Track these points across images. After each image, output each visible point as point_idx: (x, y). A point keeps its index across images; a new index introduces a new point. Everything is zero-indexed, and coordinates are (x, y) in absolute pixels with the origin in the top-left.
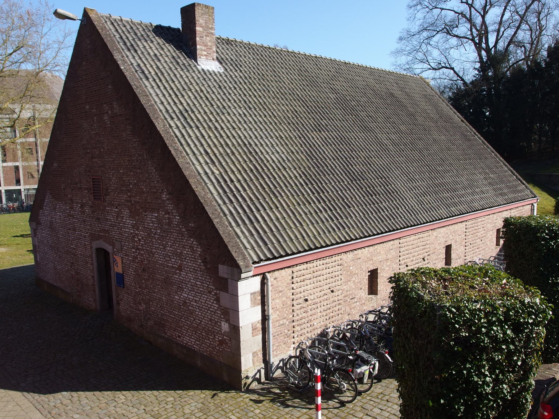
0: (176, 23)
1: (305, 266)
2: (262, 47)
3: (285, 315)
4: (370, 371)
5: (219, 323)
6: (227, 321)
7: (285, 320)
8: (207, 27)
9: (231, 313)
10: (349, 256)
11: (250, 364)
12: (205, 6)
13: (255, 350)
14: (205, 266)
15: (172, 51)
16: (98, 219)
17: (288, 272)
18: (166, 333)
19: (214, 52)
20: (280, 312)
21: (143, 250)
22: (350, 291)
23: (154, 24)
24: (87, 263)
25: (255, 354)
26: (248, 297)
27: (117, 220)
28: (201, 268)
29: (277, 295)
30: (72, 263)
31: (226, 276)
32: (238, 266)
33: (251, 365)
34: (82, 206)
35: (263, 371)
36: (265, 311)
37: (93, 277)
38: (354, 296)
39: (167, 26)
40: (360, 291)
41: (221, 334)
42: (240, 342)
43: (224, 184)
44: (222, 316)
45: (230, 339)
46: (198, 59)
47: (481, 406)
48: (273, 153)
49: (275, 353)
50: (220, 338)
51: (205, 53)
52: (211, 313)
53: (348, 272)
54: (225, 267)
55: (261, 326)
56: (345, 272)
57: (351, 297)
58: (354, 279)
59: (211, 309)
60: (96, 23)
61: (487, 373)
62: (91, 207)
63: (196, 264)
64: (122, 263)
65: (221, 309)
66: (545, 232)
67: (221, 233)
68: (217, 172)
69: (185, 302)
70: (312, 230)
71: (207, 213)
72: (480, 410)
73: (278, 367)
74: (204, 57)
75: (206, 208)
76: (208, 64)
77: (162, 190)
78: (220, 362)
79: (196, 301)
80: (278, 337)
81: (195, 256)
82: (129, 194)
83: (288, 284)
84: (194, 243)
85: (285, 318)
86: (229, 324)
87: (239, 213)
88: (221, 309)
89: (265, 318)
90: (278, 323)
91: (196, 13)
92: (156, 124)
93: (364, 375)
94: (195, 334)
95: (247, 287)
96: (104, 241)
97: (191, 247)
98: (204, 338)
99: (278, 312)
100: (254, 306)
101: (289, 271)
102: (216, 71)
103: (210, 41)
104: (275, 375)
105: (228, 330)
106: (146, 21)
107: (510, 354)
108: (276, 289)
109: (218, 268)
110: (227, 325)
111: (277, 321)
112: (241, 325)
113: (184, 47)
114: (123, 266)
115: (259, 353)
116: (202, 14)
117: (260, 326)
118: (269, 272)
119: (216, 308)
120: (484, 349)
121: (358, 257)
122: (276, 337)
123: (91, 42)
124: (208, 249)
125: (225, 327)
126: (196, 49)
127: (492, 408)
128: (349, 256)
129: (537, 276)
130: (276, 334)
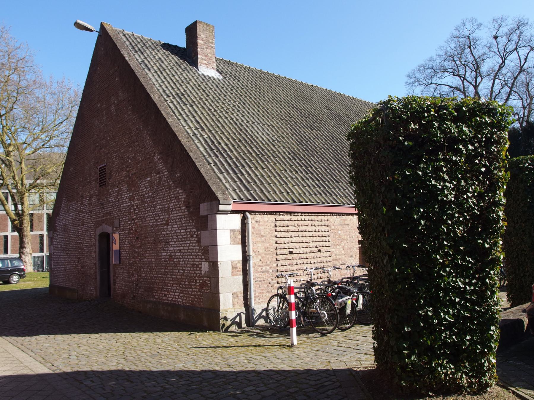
0: (182, 44)
1: (288, 217)
2: (261, 71)
3: (268, 263)
4: (352, 302)
5: (200, 266)
6: (207, 260)
7: (268, 268)
8: (208, 41)
9: (209, 252)
10: (337, 220)
11: (229, 305)
12: (206, 24)
13: (235, 291)
14: (188, 211)
15: (176, 59)
16: (102, 204)
17: (271, 219)
18: (153, 297)
19: (213, 62)
20: (262, 257)
21: (137, 219)
22: (339, 255)
23: (162, 42)
24: (91, 252)
25: (235, 296)
26: (228, 233)
27: (117, 198)
28: (184, 215)
29: (259, 239)
30: (79, 258)
31: (206, 214)
32: (216, 199)
33: (231, 306)
34: (90, 198)
35: (243, 316)
36: (246, 252)
37: (95, 264)
38: (344, 262)
39: (174, 44)
40: (351, 259)
41: (202, 277)
42: (218, 278)
43: (212, 146)
44: (203, 257)
45: (210, 278)
46: (199, 67)
47: (445, 218)
48: (262, 133)
49: (257, 299)
50: (201, 281)
51: (206, 62)
52: (193, 258)
53: (336, 235)
54: (205, 204)
55: (241, 267)
56: (332, 235)
57: (341, 263)
58: (343, 244)
59: (193, 254)
60: (109, 32)
61: (446, 176)
62: (97, 196)
63: (180, 213)
64: (120, 240)
65: (202, 250)
66: (527, 162)
67: (202, 172)
68: (206, 136)
69: (171, 256)
70: (296, 190)
71: (191, 157)
72: (445, 223)
73: (260, 316)
74: (205, 66)
75: (190, 154)
76: (207, 70)
77: (154, 153)
78: (201, 308)
79: (180, 251)
80: (260, 283)
81: (180, 205)
82: (128, 169)
83: (271, 231)
84: (180, 191)
85: (268, 265)
86: (209, 262)
87: (223, 165)
88: (202, 250)
89: (245, 260)
90: (260, 268)
91: (198, 28)
92: (152, 96)
93: (346, 304)
94: (179, 286)
95: (226, 224)
96: (106, 224)
97: (176, 197)
98: (186, 288)
99: (260, 257)
100: (234, 244)
101: (272, 217)
102: (215, 77)
103: (210, 53)
104: (258, 323)
105: (208, 270)
106: (156, 39)
107: (470, 158)
108: (257, 232)
109: (199, 208)
110: (207, 264)
111: (260, 266)
112: (219, 260)
113: (188, 59)
114: (120, 242)
115: (240, 295)
116: (203, 30)
117: (240, 266)
118: (251, 212)
119: (197, 251)
120: (439, 147)
121: (347, 222)
122: (259, 282)
123: (109, 60)
124: (191, 192)
125: (205, 266)
126: (197, 59)
127: (458, 223)
128: (337, 220)
129: (526, 209)
130: (259, 280)
